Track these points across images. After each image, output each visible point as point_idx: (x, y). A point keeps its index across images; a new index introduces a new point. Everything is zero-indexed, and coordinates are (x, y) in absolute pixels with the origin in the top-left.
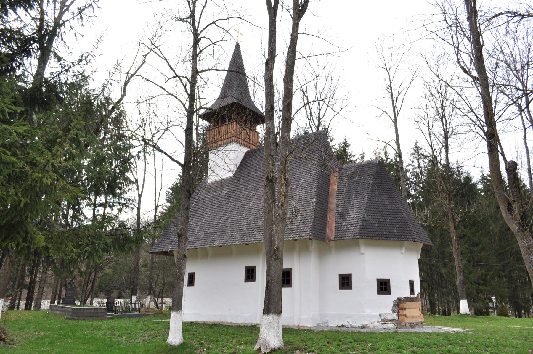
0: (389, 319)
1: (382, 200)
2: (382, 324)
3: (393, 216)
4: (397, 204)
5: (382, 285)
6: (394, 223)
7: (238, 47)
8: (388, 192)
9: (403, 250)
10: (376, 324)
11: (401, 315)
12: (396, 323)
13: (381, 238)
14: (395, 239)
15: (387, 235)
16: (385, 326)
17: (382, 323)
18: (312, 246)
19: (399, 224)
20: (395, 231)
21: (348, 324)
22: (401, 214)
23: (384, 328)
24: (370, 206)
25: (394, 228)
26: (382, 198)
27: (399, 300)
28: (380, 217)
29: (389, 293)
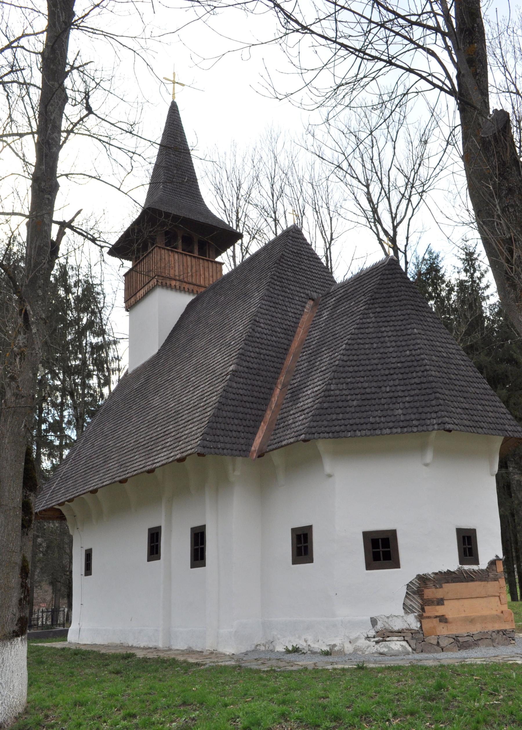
0: (396, 628)
1: (380, 345)
2: (377, 642)
3: (400, 376)
4: (417, 347)
5: (469, 549)
6: (400, 394)
7: (174, 110)
8: (400, 323)
9: (429, 457)
10: (362, 643)
11: (429, 617)
12: (413, 638)
13: (358, 433)
14: (395, 430)
15: (376, 423)
16: (382, 648)
17: (376, 639)
18: (234, 470)
19: (413, 393)
20: (400, 411)
21: (305, 644)
22: (422, 368)
23: (381, 654)
24: (348, 363)
25: (397, 406)
26: (382, 340)
27: (423, 579)
28: (366, 385)
29: (397, 565)
